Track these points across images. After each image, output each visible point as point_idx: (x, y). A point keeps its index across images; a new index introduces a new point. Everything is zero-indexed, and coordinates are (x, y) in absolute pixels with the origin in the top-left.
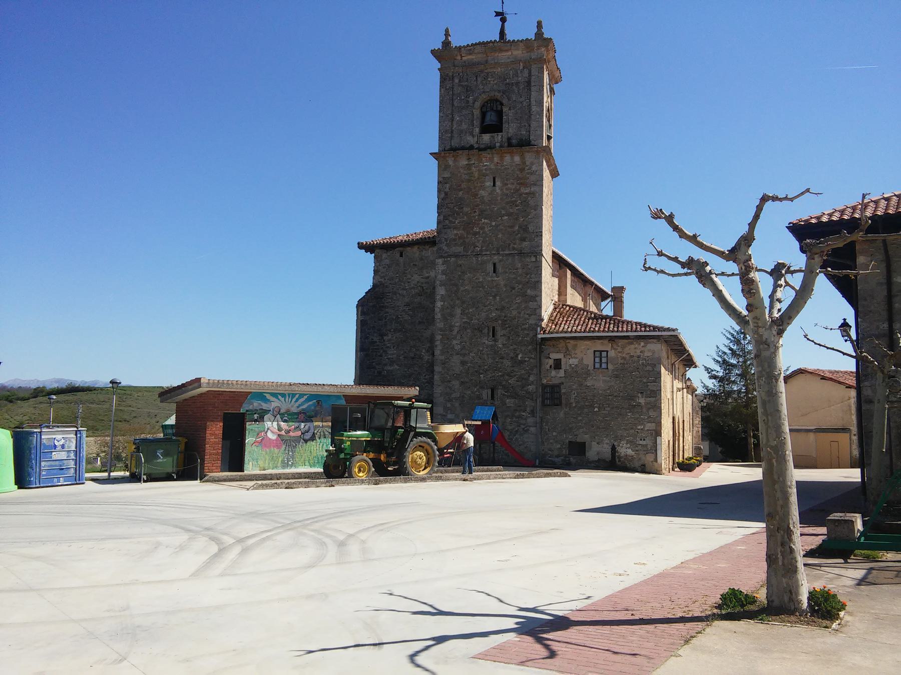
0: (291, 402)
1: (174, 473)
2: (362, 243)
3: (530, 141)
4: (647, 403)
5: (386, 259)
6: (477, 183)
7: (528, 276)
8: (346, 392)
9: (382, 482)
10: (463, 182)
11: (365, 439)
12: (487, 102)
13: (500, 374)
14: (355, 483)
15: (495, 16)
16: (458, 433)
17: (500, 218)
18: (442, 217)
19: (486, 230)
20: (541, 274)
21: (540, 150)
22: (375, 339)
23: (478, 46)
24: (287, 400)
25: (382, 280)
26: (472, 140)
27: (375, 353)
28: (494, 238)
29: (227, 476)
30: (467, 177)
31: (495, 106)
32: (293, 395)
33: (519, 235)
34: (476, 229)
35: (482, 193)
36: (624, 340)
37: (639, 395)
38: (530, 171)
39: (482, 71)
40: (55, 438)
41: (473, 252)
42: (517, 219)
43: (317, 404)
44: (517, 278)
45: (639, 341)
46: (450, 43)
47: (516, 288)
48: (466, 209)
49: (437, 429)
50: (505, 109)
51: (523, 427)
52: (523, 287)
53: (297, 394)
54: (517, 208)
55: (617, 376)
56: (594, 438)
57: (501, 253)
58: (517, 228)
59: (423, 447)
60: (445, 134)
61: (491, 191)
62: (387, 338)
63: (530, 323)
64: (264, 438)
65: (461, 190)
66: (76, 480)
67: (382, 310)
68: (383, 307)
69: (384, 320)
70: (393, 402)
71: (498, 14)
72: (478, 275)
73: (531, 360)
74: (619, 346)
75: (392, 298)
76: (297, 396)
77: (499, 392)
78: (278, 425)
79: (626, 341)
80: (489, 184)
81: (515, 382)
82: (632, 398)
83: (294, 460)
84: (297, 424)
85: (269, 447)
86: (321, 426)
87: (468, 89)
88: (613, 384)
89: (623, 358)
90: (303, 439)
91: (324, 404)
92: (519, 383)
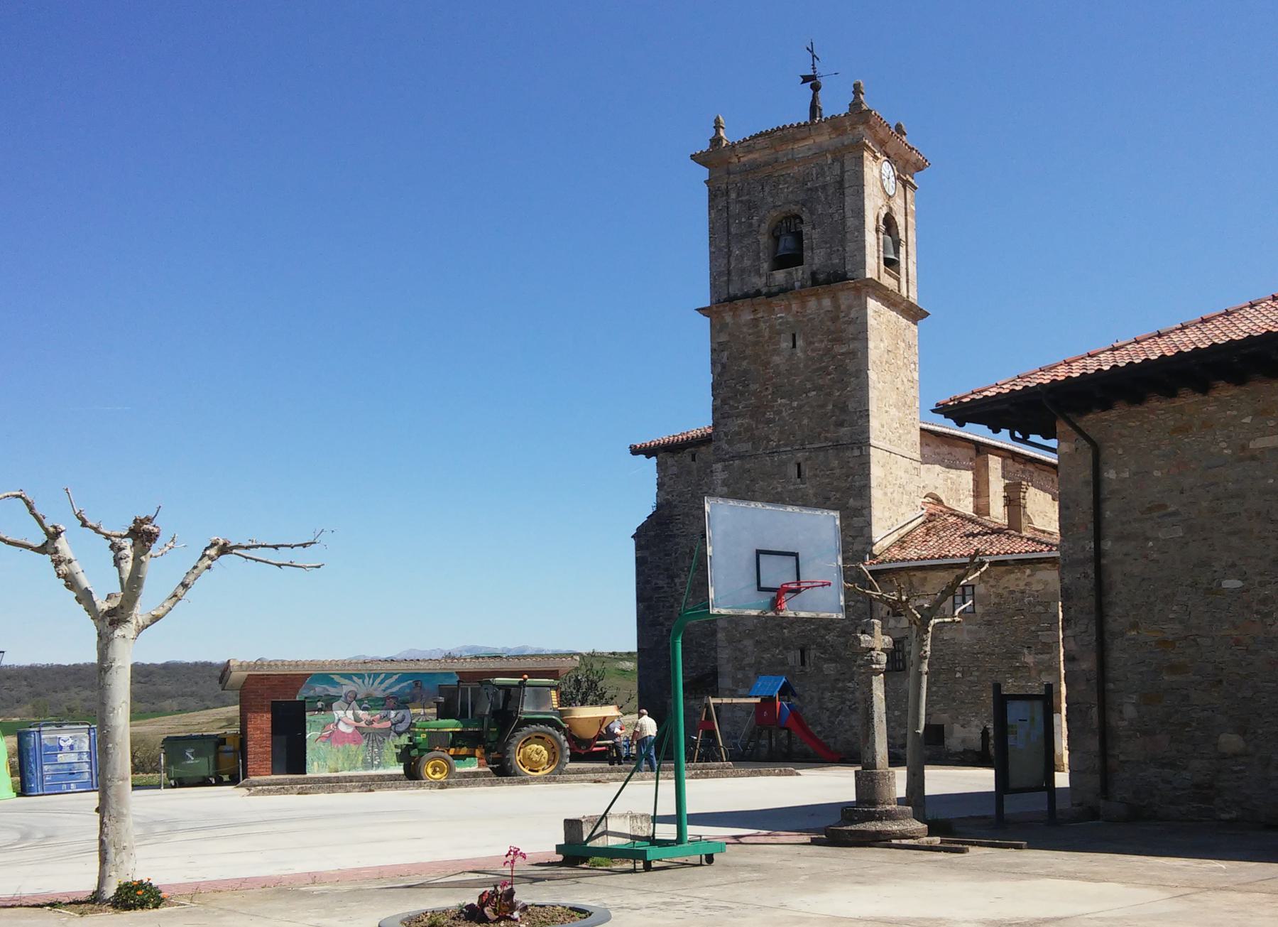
0: (373, 684)
1: (211, 777)
2: (635, 446)
3: (846, 273)
4: (1037, 662)
5: (673, 465)
6: (768, 346)
7: (849, 479)
8: (454, 667)
9: (452, 785)
10: (747, 346)
11: (451, 730)
12: (781, 222)
13: (812, 627)
14: (408, 787)
15: (803, 83)
16: (605, 718)
17: (804, 395)
18: (719, 401)
19: (784, 414)
20: (869, 474)
21: (858, 285)
22: (661, 583)
23: (760, 138)
24: (366, 681)
25: (668, 497)
26: (759, 282)
27: (662, 604)
28: (796, 426)
29: (272, 780)
30: (751, 338)
31: (793, 226)
32: (377, 675)
33: (834, 418)
34: (769, 415)
35: (776, 359)
36: (999, 568)
37: (1026, 651)
38: (847, 319)
39: (770, 176)
40: (59, 738)
41: (766, 448)
42: (830, 394)
43: (414, 685)
44: (833, 484)
45: (1022, 567)
46: (721, 139)
47: (832, 499)
48: (753, 387)
49: (570, 712)
50: (806, 229)
51: (848, 703)
52: (842, 497)
53: (381, 674)
54: (829, 377)
55: (989, 623)
56: (957, 718)
57: (808, 446)
58: (830, 407)
59: (543, 738)
60: (720, 276)
61: (789, 356)
62: (679, 581)
63: (855, 550)
64: (334, 732)
65: (745, 358)
66: (92, 786)
67: (671, 541)
68: (671, 536)
69: (673, 554)
70: (491, 680)
71: (806, 79)
72: (775, 482)
73: (859, 605)
74: (991, 577)
75: (684, 524)
76: (383, 676)
77: (813, 653)
78: (354, 714)
79: (1003, 568)
80: (785, 344)
81: (835, 638)
82: (1014, 655)
83: (382, 758)
84: (383, 713)
85: (343, 743)
86: (422, 713)
87: (751, 207)
88: (983, 635)
89: (1001, 596)
90: (395, 732)
91: (425, 685)
92: (842, 640)
